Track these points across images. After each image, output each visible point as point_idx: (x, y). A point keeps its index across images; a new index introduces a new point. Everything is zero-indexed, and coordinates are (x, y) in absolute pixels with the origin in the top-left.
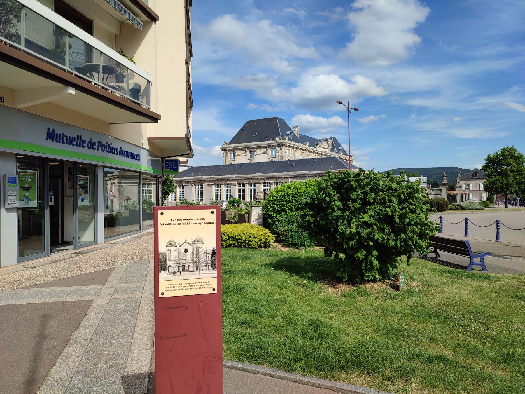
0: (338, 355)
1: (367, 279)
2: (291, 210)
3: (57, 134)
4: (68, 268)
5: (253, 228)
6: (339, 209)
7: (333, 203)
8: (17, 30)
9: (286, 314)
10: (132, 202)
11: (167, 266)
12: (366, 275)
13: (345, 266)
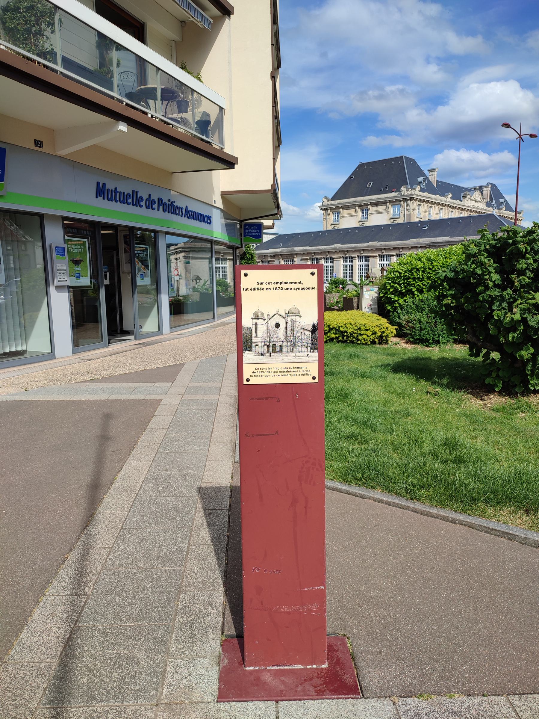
0: (483, 485)
1: (532, 388)
2: (421, 291)
3: (108, 190)
4: (129, 361)
5: (365, 317)
6: (496, 286)
7: (487, 277)
8: (51, 45)
9: (409, 429)
10: (202, 282)
11: (253, 345)
12: (532, 382)
13: (499, 369)
